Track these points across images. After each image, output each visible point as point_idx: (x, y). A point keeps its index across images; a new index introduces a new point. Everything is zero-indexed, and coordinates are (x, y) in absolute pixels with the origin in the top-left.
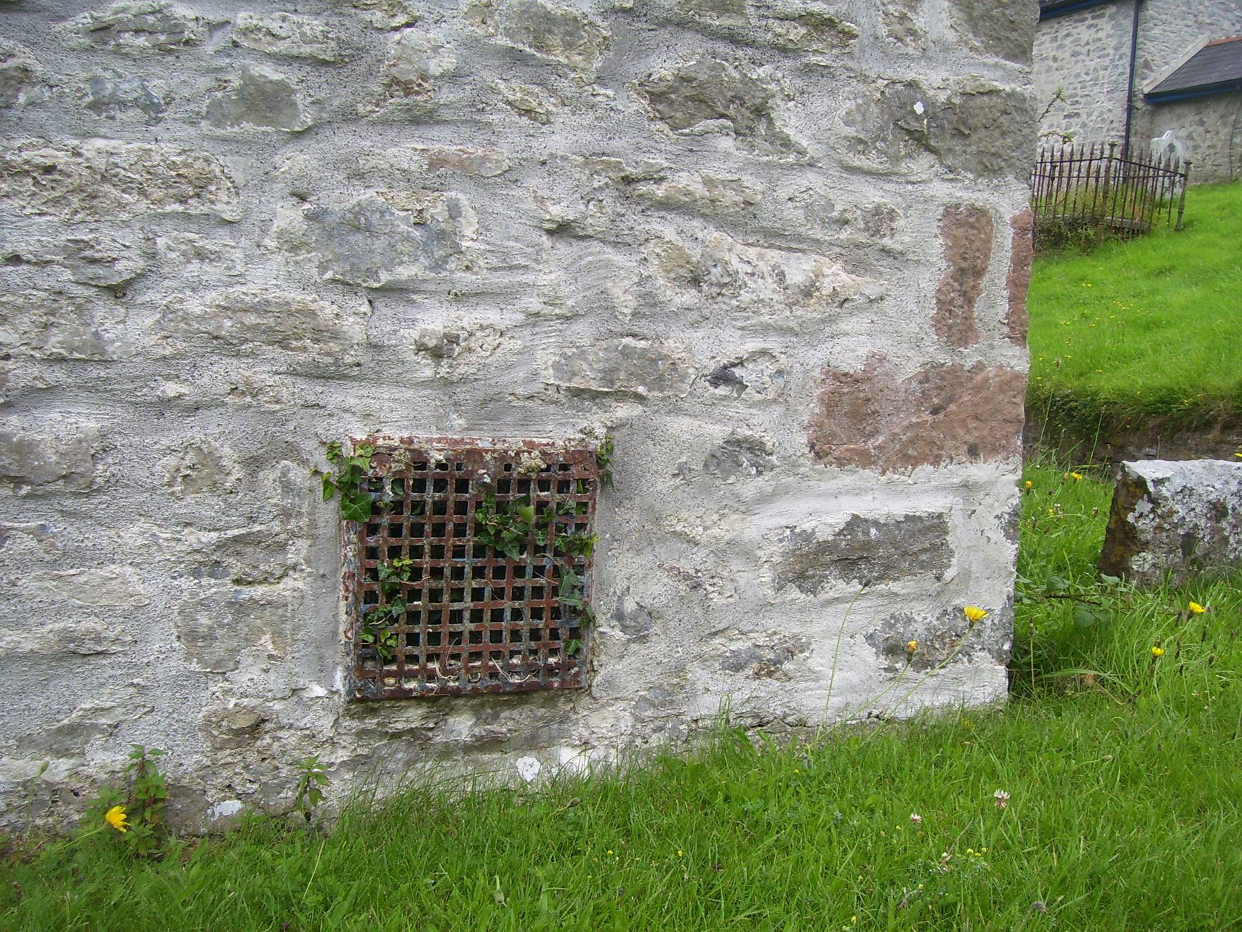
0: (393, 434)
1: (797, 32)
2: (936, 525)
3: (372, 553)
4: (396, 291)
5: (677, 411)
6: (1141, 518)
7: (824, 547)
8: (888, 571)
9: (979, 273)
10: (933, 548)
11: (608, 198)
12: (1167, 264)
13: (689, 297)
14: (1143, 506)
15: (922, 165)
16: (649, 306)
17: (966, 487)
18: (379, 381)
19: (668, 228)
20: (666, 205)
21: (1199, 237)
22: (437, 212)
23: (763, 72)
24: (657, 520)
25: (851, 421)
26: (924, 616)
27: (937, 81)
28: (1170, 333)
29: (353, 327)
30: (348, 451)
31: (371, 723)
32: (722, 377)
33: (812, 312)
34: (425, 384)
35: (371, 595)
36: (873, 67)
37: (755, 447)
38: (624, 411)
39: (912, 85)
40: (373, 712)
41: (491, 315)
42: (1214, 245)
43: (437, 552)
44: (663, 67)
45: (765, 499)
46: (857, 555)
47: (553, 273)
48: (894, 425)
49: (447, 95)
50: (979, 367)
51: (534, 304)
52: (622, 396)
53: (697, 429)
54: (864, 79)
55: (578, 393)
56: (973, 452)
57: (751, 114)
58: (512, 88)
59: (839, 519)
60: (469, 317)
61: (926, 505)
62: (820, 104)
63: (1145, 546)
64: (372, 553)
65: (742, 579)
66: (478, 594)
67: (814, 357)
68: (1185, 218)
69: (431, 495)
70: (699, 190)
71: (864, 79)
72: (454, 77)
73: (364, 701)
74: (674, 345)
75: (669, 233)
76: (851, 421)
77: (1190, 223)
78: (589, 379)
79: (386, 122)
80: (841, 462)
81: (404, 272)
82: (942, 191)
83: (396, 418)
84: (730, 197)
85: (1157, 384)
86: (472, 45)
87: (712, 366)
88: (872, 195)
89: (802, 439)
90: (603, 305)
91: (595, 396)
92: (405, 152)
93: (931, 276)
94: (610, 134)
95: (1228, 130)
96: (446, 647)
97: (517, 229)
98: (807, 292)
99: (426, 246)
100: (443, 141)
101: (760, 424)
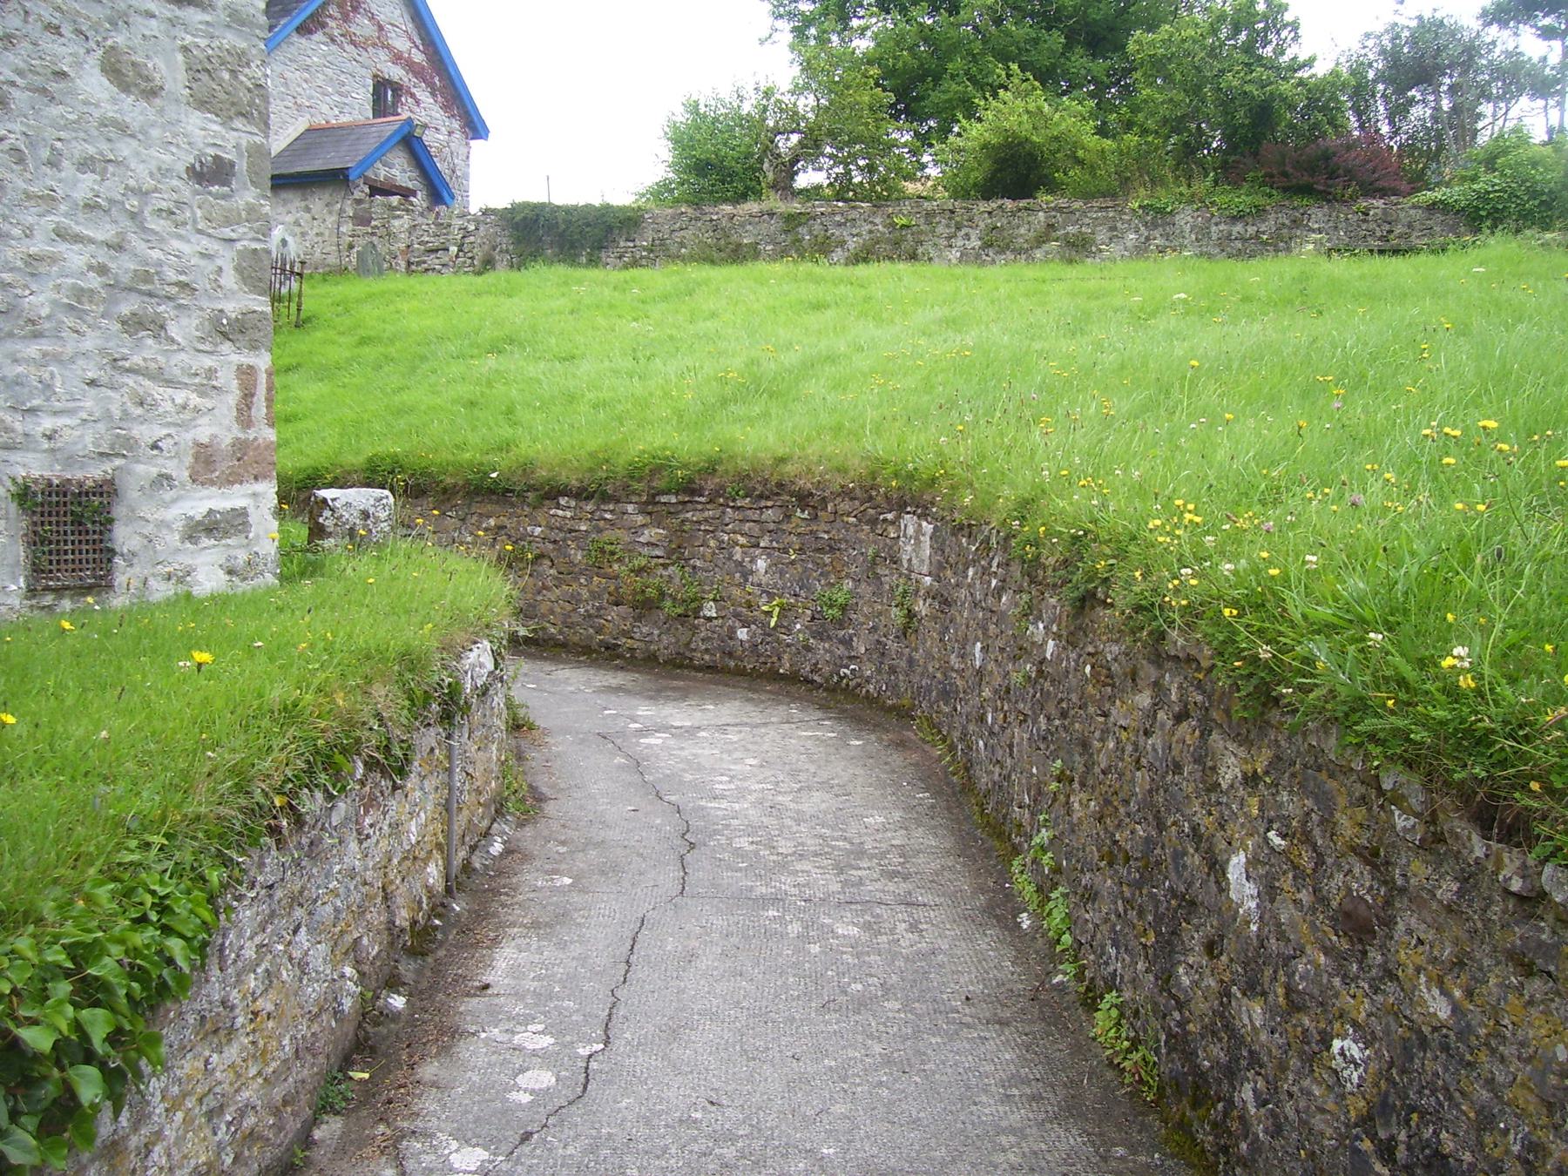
0: (36, 473)
1: (174, 290)
2: (242, 513)
3: (35, 524)
4: (32, 411)
5: (138, 462)
6: (326, 519)
7: (199, 523)
8: (226, 534)
9: (253, 395)
10: (244, 523)
11: (108, 368)
12: (294, 362)
13: (139, 411)
14: (327, 513)
15: (226, 347)
16: (126, 415)
17: (255, 495)
18: (28, 450)
19: (130, 380)
20: (128, 370)
21: (319, 334)
22: (46, 376)
23: (161, 309)
24: (133, 511)
25: (206, 465)
26: (242, 556)
27: (232, 308)
28: (309, 424)
29: (18, 426)
30: (20, 481)
31: (34, 602)
32: (155, 446)
33: (187, 416)
34: (45, 451)
35: (36, 540)
36: (205, 304)
37: (168, 478)
38: (118, 462)
39: (221, 311)
40: (34, 596)
41: (68, 421)
42: (333, 342)
43: (58, 523)
44: (125, 310)
45: (174, 501)
46: (211, 527)
47: (90, 402)
48: (223, 466)
49: (47, 325)
50: (256, 439)
51: (85, 416)
52: (117, 455)
53: (146, 470)
54: (201, 309)
55: (101, 454)
56: (256, 478)
57: (157, 327)
58: (69, 321)
59: (204, 510)
60: (60, 422)
61: (239, 503)
62: (184, 321)
63: (330, 535)
64: (35, 524)
65: (168, 538)
66: (73, 542)
67: (188, 436)
68: (303, 315)
69: (55, 499)
70: (142, 363)
71: (201, 309)
72: (49, 317)
73: (32, 592)
74: (135, 432)
75: (131, 383)
76: (206, 465)
77: (308, 320)
78: (105, 449)
79: (25, 337)
80: (203, 484)
81: (36, 402)
82: (236, 358)
83: (34, 466)
84: (153, 365)
85: (304, 465)
86: (55, 303)
87: (151, 442)
88: (208, 362)
89: (187, 474)
90: (108, 415)
91: (108, 455)
92: (32, 350)
93: (233, 398)
94: (107, 340)
95: (334, 218)
96: (63, 566)
97: (75, 383)
98: (184, 407)
99: (43, 392)
100: (46, 345)
101: (171, 468)
